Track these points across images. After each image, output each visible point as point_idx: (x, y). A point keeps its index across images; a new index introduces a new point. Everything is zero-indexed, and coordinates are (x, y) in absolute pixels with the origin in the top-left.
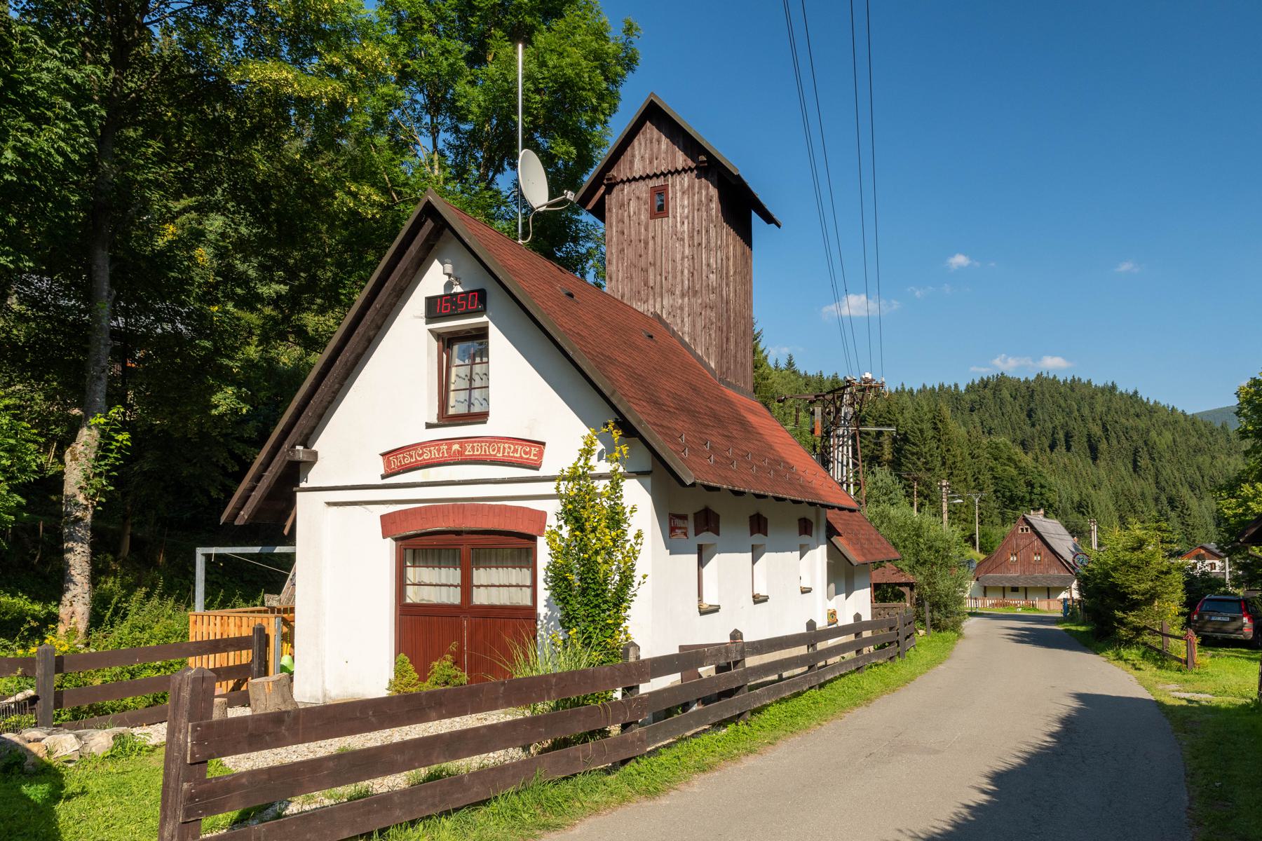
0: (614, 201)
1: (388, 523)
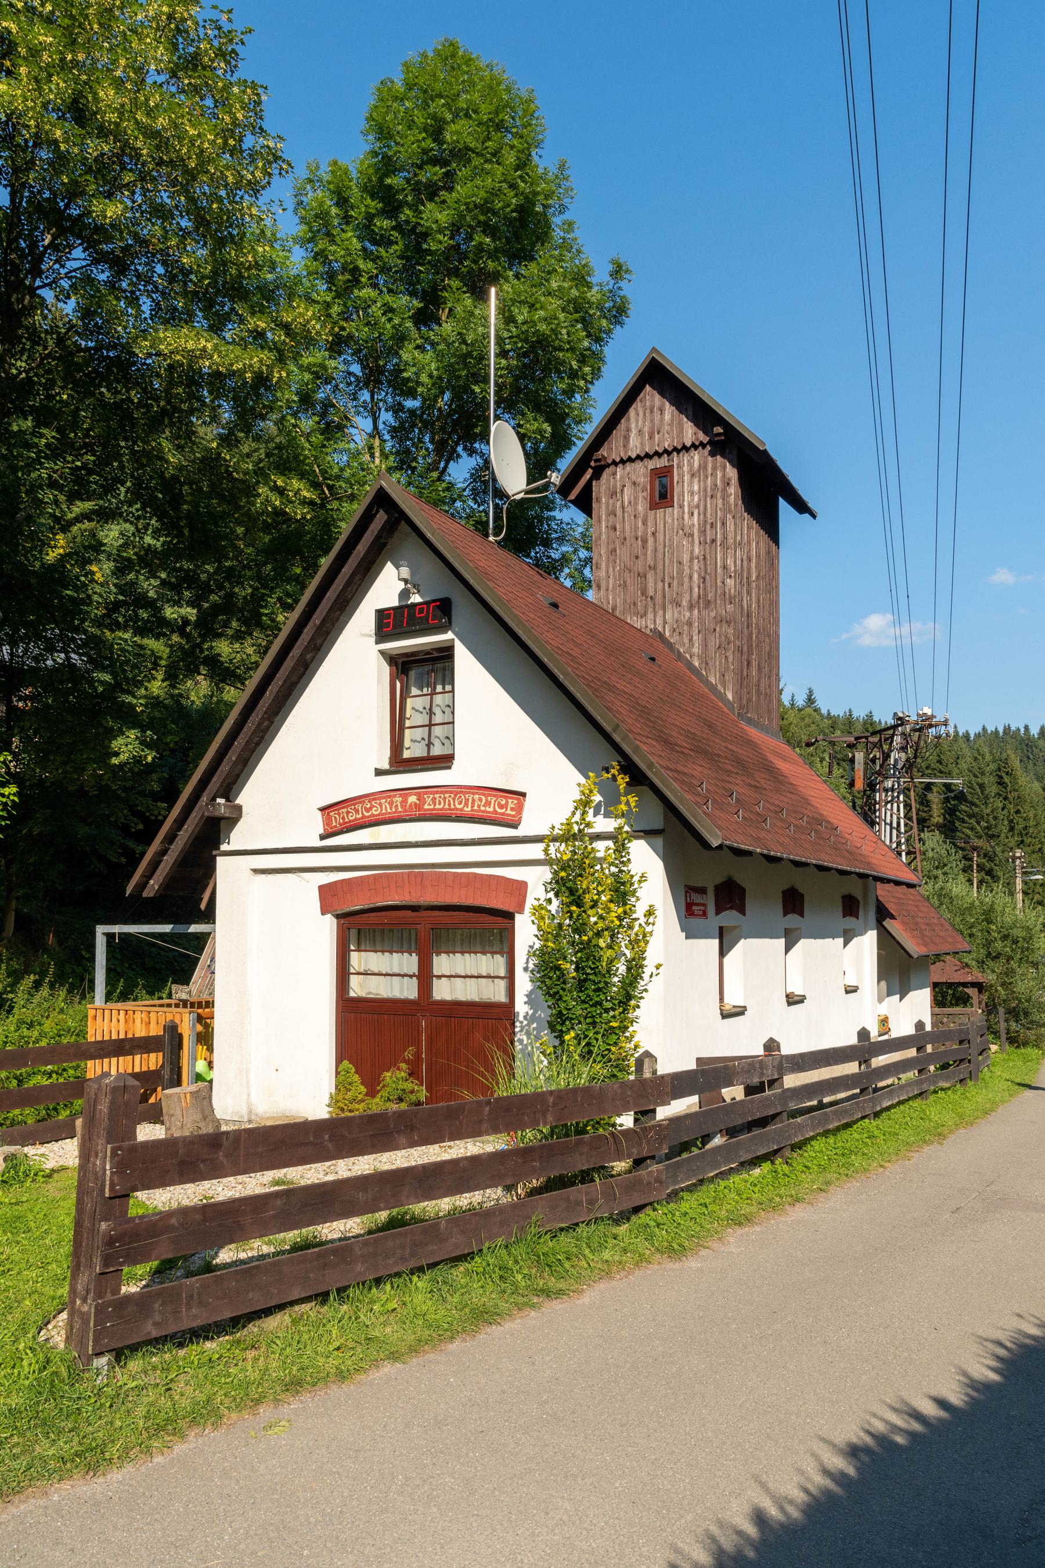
0: (603, 488)
1: (328, 896)
